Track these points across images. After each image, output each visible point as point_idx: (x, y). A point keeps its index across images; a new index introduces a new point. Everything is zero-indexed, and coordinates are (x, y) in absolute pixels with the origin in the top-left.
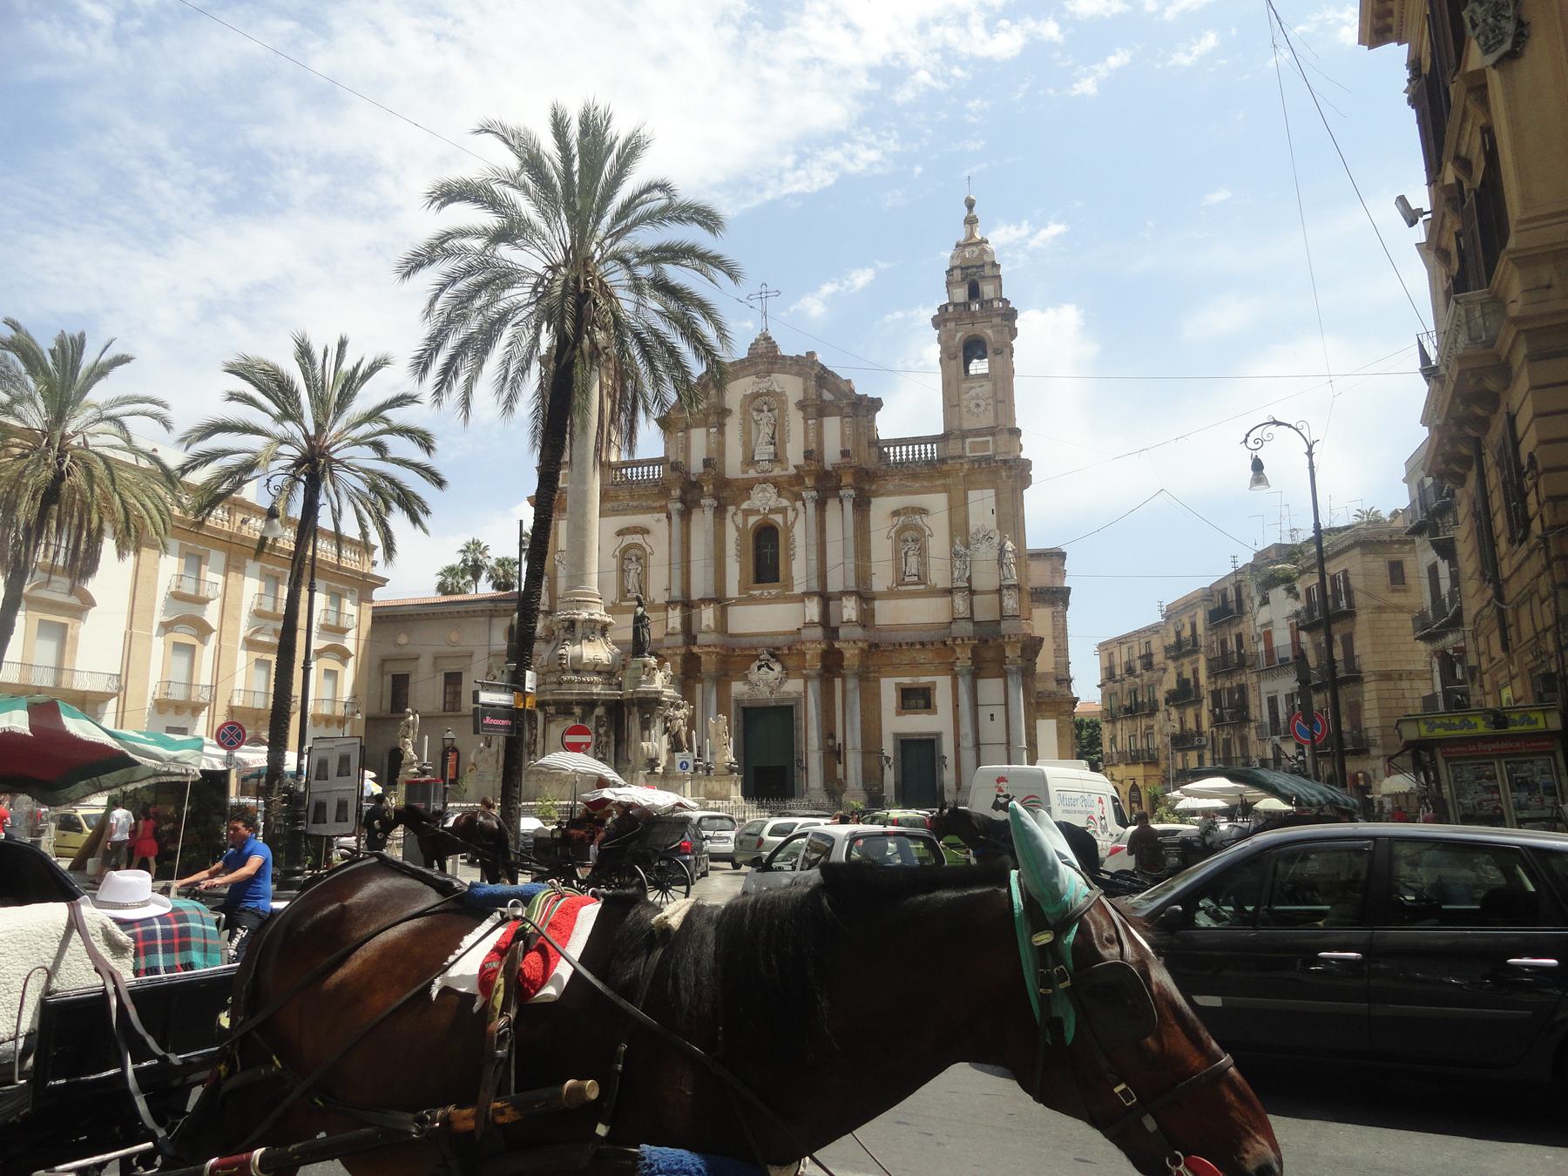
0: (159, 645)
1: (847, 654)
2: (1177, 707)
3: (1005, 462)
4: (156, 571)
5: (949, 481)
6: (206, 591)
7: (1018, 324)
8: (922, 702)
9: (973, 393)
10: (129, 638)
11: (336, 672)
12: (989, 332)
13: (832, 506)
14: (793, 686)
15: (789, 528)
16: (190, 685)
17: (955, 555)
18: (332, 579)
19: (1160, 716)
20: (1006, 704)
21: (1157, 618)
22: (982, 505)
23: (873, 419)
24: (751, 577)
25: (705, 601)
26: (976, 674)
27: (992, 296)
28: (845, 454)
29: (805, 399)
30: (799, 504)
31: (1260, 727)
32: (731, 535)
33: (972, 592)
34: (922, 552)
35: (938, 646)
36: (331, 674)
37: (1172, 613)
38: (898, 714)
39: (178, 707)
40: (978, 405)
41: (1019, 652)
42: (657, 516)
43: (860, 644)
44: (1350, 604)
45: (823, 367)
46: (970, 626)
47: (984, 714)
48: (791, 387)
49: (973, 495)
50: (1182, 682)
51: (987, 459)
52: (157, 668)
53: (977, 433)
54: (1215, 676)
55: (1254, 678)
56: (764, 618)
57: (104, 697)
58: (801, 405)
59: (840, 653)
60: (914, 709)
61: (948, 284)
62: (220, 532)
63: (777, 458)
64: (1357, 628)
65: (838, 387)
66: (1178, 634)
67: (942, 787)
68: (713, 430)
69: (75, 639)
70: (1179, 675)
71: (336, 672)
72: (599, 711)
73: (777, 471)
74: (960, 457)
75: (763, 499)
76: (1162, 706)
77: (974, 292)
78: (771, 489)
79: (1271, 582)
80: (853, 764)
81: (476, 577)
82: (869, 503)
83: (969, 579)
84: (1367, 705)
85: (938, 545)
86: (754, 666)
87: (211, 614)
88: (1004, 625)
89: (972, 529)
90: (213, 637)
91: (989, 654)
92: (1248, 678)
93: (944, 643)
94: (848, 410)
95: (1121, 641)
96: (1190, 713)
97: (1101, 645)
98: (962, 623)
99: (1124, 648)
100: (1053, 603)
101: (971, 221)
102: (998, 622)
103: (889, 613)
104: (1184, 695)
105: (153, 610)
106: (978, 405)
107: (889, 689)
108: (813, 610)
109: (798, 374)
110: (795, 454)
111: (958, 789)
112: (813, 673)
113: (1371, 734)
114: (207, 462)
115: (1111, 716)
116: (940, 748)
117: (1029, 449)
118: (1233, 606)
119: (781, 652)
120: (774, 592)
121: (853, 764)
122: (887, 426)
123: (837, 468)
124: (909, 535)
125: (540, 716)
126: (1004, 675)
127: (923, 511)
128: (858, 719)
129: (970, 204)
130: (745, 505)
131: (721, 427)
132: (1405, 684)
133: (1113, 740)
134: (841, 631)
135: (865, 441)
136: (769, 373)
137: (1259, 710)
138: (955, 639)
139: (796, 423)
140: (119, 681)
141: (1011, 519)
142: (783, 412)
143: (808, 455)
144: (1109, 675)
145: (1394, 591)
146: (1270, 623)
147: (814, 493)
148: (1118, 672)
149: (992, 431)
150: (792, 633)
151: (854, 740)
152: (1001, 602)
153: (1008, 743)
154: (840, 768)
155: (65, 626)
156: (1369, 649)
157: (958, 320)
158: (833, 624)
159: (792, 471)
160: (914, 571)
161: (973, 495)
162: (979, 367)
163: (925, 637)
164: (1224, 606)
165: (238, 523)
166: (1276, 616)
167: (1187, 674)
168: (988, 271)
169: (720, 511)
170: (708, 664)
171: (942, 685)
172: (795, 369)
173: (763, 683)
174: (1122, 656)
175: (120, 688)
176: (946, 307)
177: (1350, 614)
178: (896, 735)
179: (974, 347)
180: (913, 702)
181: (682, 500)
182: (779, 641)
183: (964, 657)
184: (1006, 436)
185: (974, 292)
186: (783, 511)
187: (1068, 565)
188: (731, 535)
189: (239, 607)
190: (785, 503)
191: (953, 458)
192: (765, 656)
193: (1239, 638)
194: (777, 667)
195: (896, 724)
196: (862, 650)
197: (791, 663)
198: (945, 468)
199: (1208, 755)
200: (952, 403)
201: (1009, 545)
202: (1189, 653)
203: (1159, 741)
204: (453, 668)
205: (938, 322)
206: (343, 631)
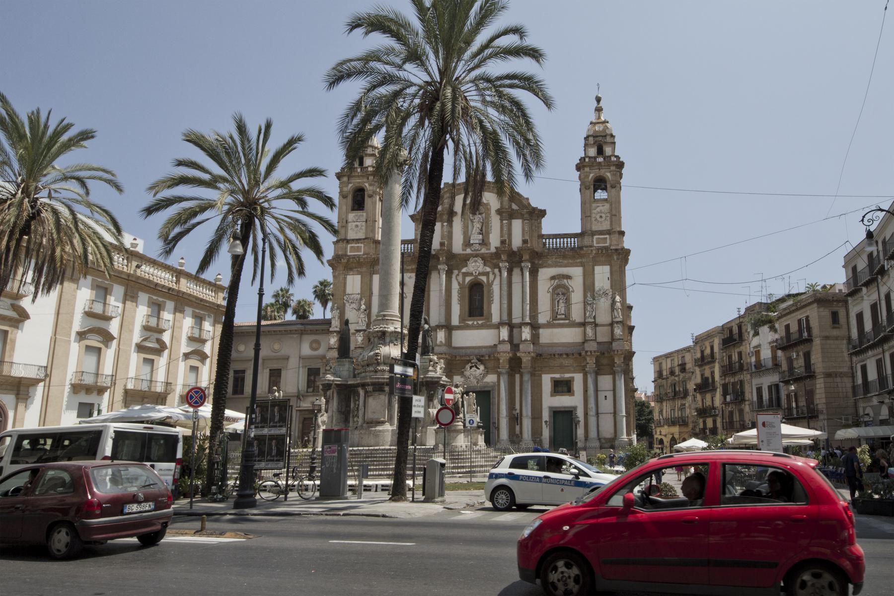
0: (75, 348)
1: (524, 360)
2: (700, 393)
3: (616, 250)
4: (75, 297)
6: (110, 312)
7: (624, 171)
8: (565, 389)
9: (598, 209)
10: (54, 341)
11: (197, 368)
12: (609, 174)
13: (516, 272)
14: (491, 378)
15: (490, 285)
16: (97, 374)
17: (585, 303)
18: (196, 308)
19: (690, 398)
21: (690, 343)
23: (540, 223)
24: (467, 314)
25: (440, 327)
26: (597, 373)
27: (610, 153)
28: (525, 242)
29: (502, 207)
30: (496, 271)
31: (752, 404)
32: (455, 286)
33: (596, 325)
34: (568, 302)
35: (575, 355)
36: (194, 369)
37: (699, 340)
38: (552, 395)
39: (88, 389)
40: (601, 217)
43: (532, 354)
44: (810, 335)
47: (601, 396)
49: (598, 269)
50: (705, 380)
51: (606, 248)
52: (74, 361)
53: (601, 233)
54: (725, 376)
55: (749, 376)
57: (35, 382)
58: (499, 212)
59: (520, 359)
62: (122, 272)
63: (485, 243)
64: (813, 349)
65: (521, 202)
66: (702, 352)
69: (13, 342)
70: (702, 375)
71: (197, 368)
73: (484, 251)
74: (591, 246)
75: (475, 267)
76: (691, 392)
77: (600, 151)
78: (480, 262)
79: (758, 324)
80: (527, 424)
81: (285, 312)
83: (594, 317)
84: (818, 391)
85: (577, 296)
86: (468, 367)
87: (114, 327)
88: (614, 344)
89: (597, 289)
90: (114, 343)
91: (605, 361)
92: (745, 376)
93: (580, 354)
94: (526, 216)
95: (667, 356)
96: (708, 396)
97: (654, 358)
98: (591, 342)
99: (669, 360)
101: (599, 110)
102: (611, 343)
103: (547, 336)
104: (705, 386)
105: (71, 323)
106: (601, 217)
107: (547, 380)
108: (504, 333)
110: (495, 240)
112: (504, 371)
113: (820, 407)
114: (167, 206)
115: (659, 398)
118: (736, 337)
119: (485, 357)
120: (480, 322)
122: (548, 226)
123: (520, 249)
124: (560, 291)
125: (362, 393)
126: (613, 373)
127: (569, 277)
128: (530, 398)
129: (598, 100)
130: (464, 270)
132: (838, 380)
133: (661, 412)
134: (521, 346)
135: (536, 235)
137: (751, 395)
138: (586, 352)
139: (495, 222)
140: (46, 371)
142: (488, 216)
143: (503, 242)
144: (659, 375)
145: (834, 328)
146: (759, 346)
148: (665, 373)
149: (609, 232)
150: (490, 347)
151: (527, 411)
154: (518, 428)
155: (6, 332)
156: (820, 360)
157: (591, 166)
158: (516, 341)
159: (493, 250)
161: (598, 269)
162: (601, 195)
163: (568, 350)
164: (731, 336)
165: (134, 267)
166: (763, 342)
167: (707, 374)
168: (608, 139)
169: (449, 274)
171: (578, 378)
174: (667, 365)
175: (46, 376)
176: (584, 158)
177: (809, 340)
178: (550, 408)
179: (600, 183)
180: (560, 389)
182: (483, 351)
183: (591, 362)
184: (617, 235)
185: (600, 151)
186: (487, 274)
188: (455, 286)
189: (133, 324)
190: (488, 269)
191: (587, 247)
192: (475, 360)
193: (740, 354)
194: (482, 367)
195: (551, 401)
196: (533, 358)
197: (491, 364)
198: (582, 252)
199: (719, 420)
200: (586, 215)
201: (618, 298)
202: (709, 363)
203: (690, 413)
204: (275, 366)
205: (579, 168)
206: (203, 341)
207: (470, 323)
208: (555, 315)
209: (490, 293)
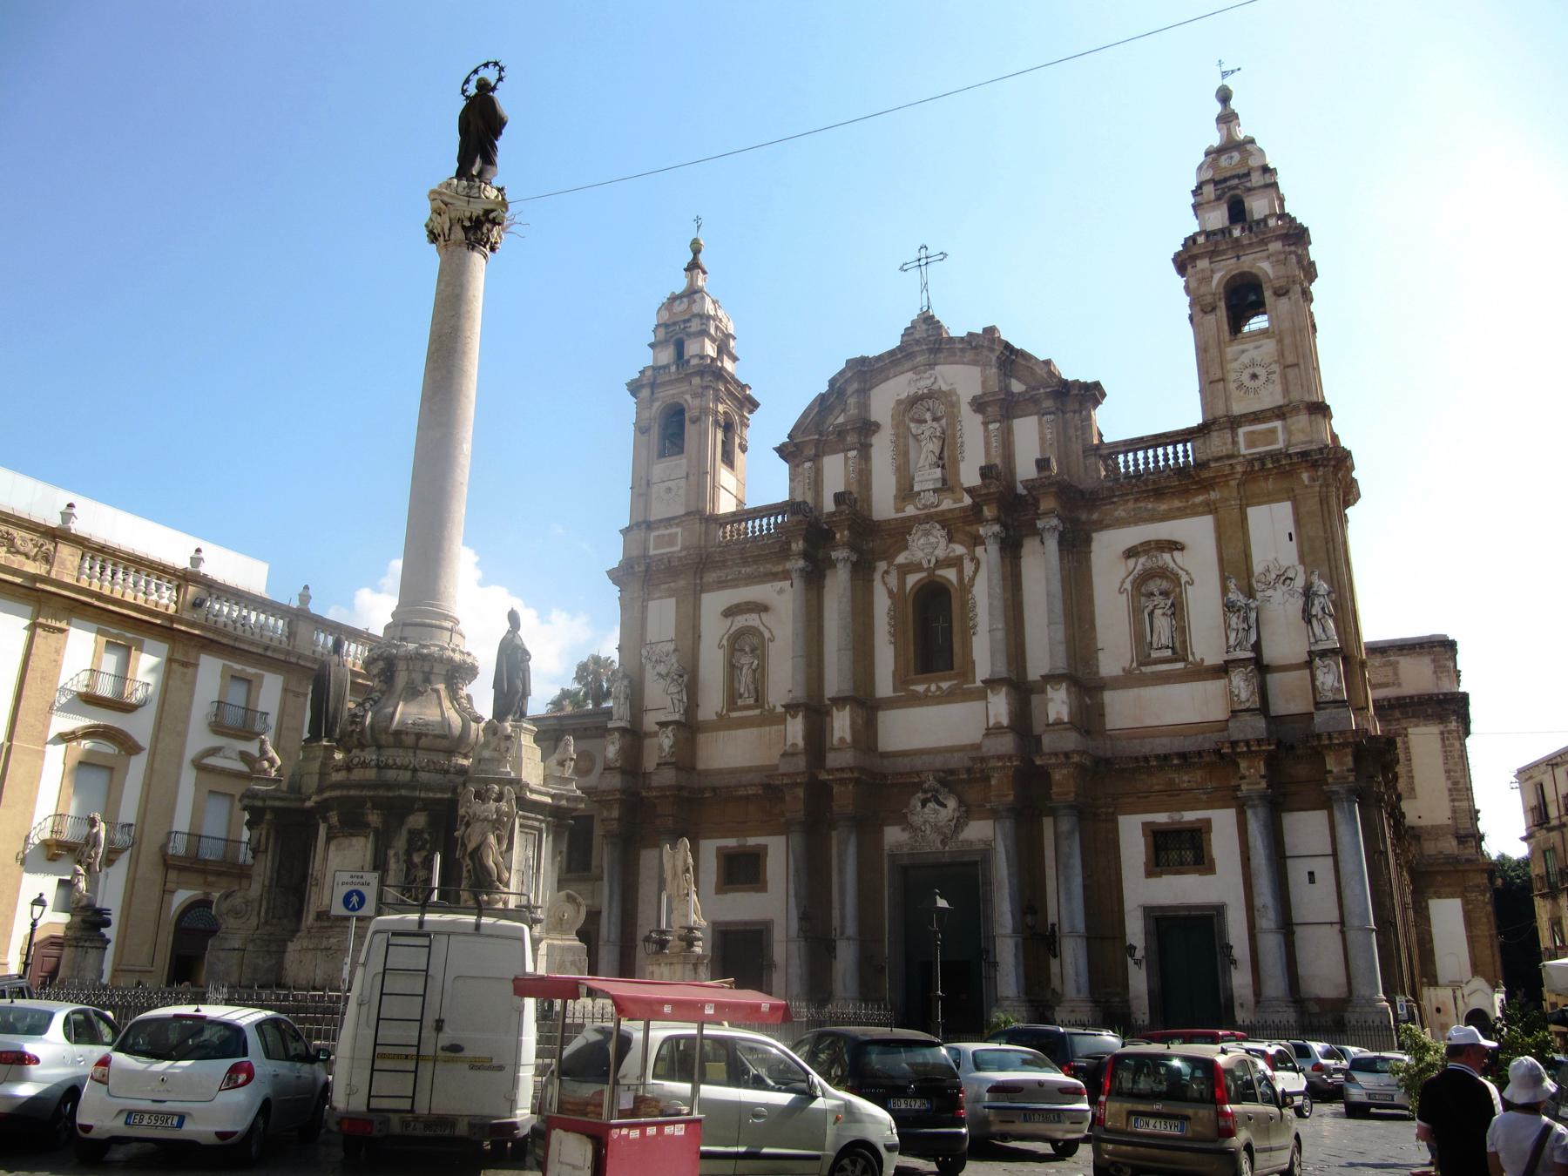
1: (1057, 776)
3: (1304, 454)
5: (1213, 495)
9: (1245, 359)
14: (978, 831)
15: (966, 587)
20: (1335, 855)
22: (1271, 528)
26: (1277, 804)
28: (1042, 464)
32: (882, 603)
34: (1177, 610)
35: (1207, 762)
38: (1149, 874)
40: (1254, 376)
41: (1349, 761)
42: (779, 585)
43: (1076, 759)
45: (1007, 346)
46: (1260, 723)
47: (1297, 872)
48: (965, 380)
49: (1254, 513)
51: (1275, 456)
53: (1256, 417)
56: (932, 727)
58: (979, 405)
60: (1179, 868)
61: (1196, 207)
67: (1230, 998)
68: (853, 454)
72: (418, 820)
73: (947, 504)
75: (927, 547)
77: (1237, 212)
78: (939, 534)
80: (1071, 964)
82: (1088, 541)
83: (1257, 647)
86: (916, 802)
89: (1258, 568)
94: (1048, 404)
98: (1247, 717)
100: (1441, 718)
103: (1126, 710)
106: (1254, 376)
109: (975, 363)
111: (1257, 1002)
116: (1223, 932)
117: (1347, 428)
119: (959, 777)
120: (945, 685)
121: (1071, 964)
124: (1155, 586)
126: (1325, 802)
127: (1174, 546)
131: (865, 450)
135: (1077, 448)
136: (932, 365)
138: (1234, 744)
141: (1326, 555)
142: (953, 418)
147: (996, 528)
148: (1553, 812)
152: (1313, 678)
153: (1342, 922)
157: (1213, 254)
160: (1165, 640)
163: (1189, 745)
168: (1257, 179)
169: (862, 571)
170: (844, 799)
171: (1223, 822)
172: (969, 355)
173: (926, 829)
179: (1242, 298)
180: (1174, 855)
181: (806, 555)
182: (955, 761)
183: (1253, 776)
185: (1237, 212)
186: (956, 562)
187: (1462, 661)
188: (882, 603)
190: (959, 550)
195: (1145, 890)
198: (1205, 474)
200: (1212, 379)
207: (921, 688)
208: (732, 698)
209: (967, 607)
